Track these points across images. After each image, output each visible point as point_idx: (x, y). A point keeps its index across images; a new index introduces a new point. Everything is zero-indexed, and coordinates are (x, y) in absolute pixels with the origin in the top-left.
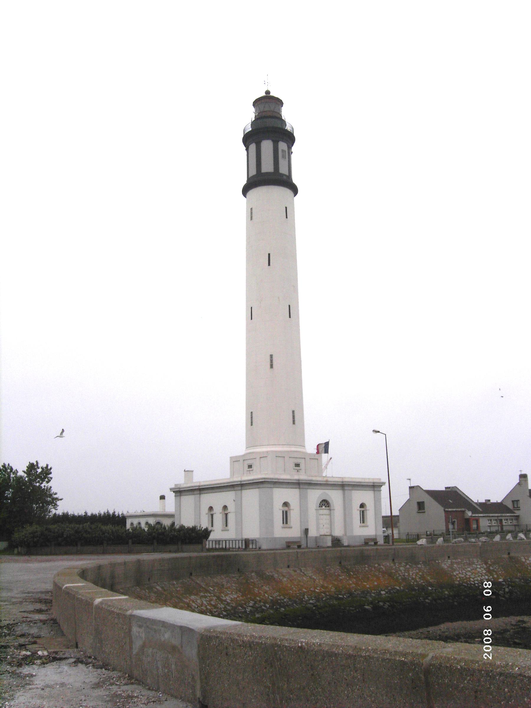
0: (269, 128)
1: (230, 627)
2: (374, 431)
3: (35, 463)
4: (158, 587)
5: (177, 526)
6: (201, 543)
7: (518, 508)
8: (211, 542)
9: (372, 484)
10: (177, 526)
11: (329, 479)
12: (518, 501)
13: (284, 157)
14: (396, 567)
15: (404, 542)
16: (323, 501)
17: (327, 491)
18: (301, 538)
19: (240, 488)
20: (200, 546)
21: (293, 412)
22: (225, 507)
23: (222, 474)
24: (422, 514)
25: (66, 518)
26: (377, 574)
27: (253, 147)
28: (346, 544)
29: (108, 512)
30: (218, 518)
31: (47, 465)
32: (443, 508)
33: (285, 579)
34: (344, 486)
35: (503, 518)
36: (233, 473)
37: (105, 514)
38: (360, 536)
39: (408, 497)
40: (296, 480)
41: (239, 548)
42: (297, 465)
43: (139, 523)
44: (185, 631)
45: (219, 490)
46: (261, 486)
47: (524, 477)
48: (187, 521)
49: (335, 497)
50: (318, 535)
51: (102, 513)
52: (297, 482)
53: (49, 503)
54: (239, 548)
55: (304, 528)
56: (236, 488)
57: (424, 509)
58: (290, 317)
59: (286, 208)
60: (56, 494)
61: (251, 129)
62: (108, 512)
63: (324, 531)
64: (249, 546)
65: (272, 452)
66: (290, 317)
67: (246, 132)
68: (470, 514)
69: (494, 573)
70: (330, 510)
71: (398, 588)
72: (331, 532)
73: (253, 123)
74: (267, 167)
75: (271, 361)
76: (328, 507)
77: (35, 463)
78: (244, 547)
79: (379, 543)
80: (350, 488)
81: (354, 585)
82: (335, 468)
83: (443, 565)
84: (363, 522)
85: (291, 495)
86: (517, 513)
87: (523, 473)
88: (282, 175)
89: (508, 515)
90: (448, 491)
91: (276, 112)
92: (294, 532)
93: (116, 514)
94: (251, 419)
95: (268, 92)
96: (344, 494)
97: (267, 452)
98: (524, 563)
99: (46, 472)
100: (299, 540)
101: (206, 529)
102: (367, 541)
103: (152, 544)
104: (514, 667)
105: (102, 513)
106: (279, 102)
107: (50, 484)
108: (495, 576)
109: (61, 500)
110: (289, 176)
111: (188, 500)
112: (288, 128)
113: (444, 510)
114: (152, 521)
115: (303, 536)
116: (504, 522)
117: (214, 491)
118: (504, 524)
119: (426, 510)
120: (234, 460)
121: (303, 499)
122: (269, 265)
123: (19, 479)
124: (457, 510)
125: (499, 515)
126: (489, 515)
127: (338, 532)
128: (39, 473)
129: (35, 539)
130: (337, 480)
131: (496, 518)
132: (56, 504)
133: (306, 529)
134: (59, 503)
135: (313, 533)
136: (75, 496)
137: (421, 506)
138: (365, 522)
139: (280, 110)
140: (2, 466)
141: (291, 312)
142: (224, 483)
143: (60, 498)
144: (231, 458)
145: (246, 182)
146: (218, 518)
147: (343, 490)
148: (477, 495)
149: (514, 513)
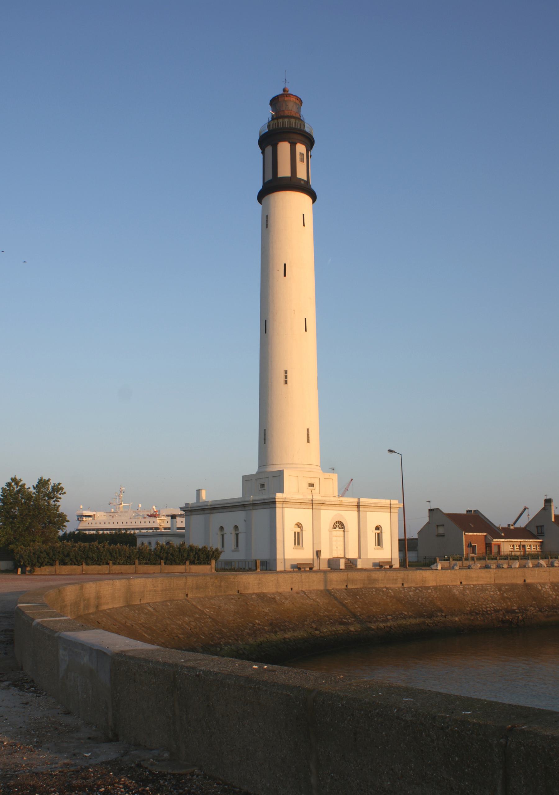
1: (152, 651)
4: (149, 608)
5: (187, 546)
10: (187, 546)
13: (302, 160)
14: (405, 592)
16: (339, 522)
17: (342, 513)
21: (308, 430)
22: (236, 527)
26: (385, 598)
27: (269, 149)
28: (359, 567)
30: (230, 539)
33: (287, 602)
39: (427, 520)
42: (312, 485)
43: (150, 543)
44: (99, 654)
47: (548, 501)
48: (196, 541)
56: (247, 508)
59: (304, 215)
61: (267, 130)
63: (338, 553)
69: (508, 600)
71: (406, 613)
76: (342, 528)
79: (394, 567)
81: (359, 609)
83: (455, 591)
84: (379, 545)
87: (548, 498)
89: (531, 540)
98: (540, 591)
101: (217, 550)
102: (379, 566)
103: (185, 564)
104: (393, 708)
108: (509, 603)
110: (308, 182)
111: (198, 519)
112: (307, 129)
114: (162, 541)
115: (315, 557)
116: (527, 548)
117: (225, 510)
120: (246, 479)
121: (315, 519)
125: (522, 540)
127: (352, 554)
135: (325, 555)
144: (243, 477)
145: (261, 188)
146: (230, 539)
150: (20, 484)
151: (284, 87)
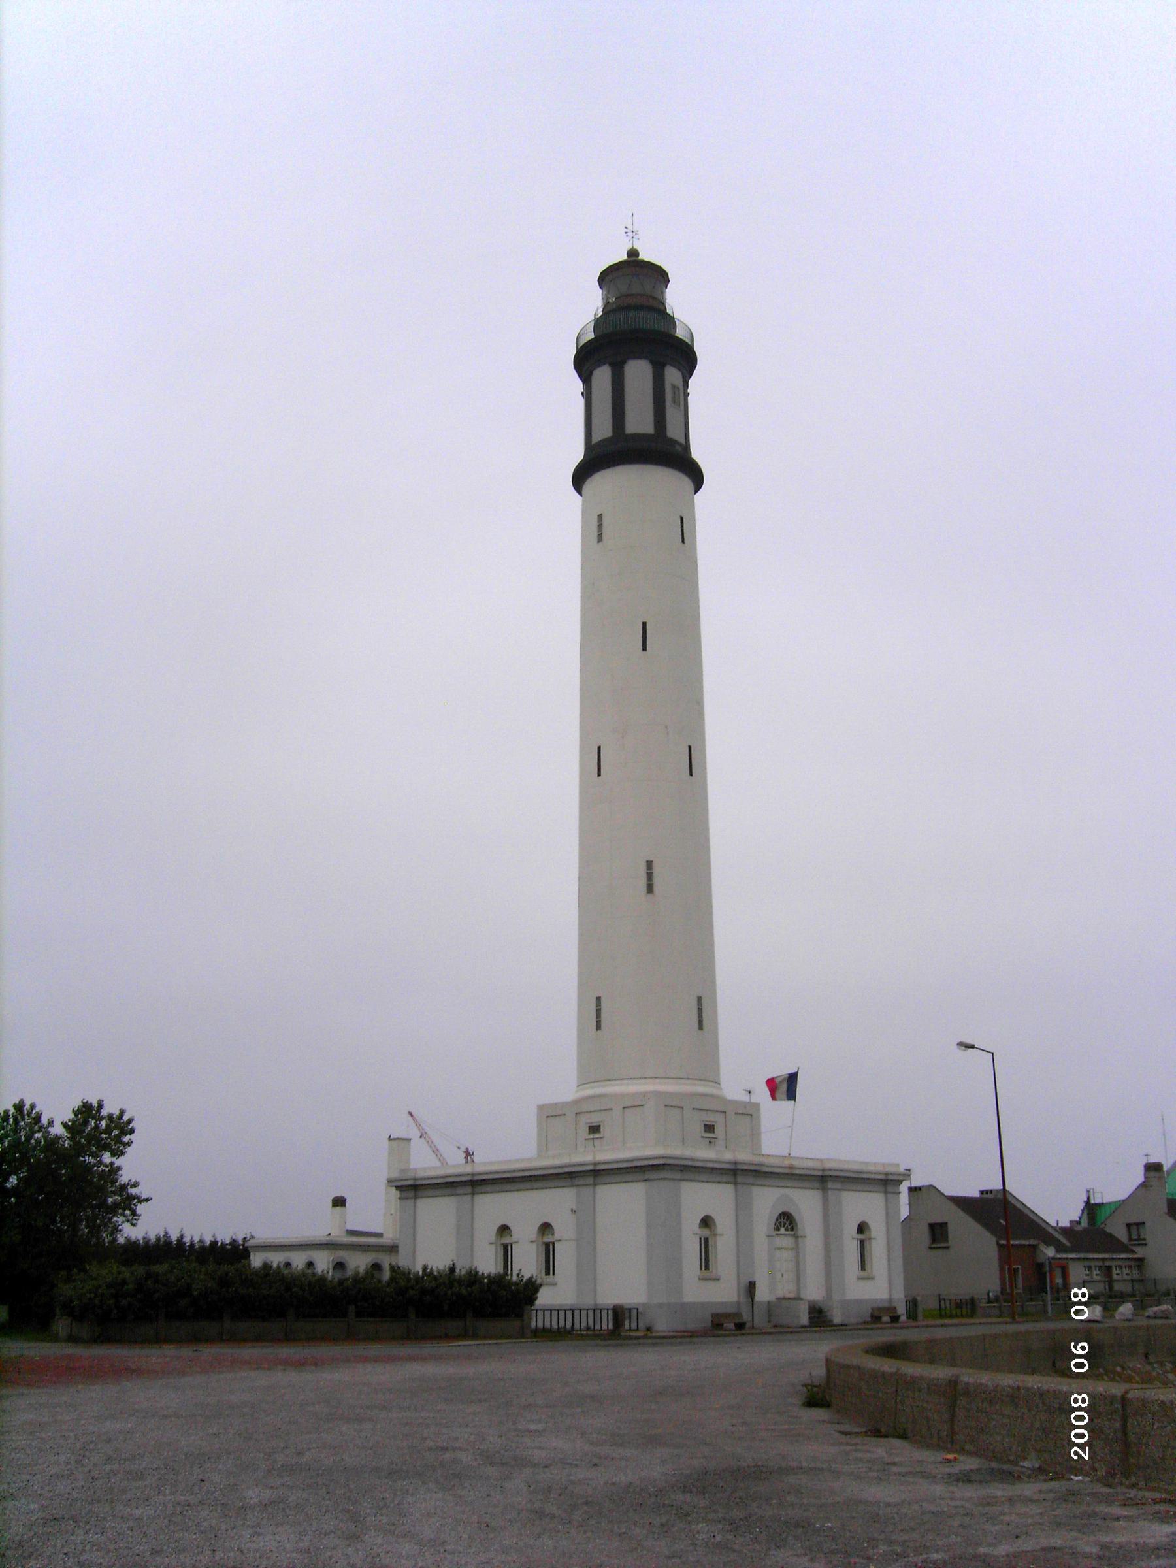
0: (635, 339)
2: (960, 1044)
3: (95, 1104)
6: (520, 1315)
7: (1142, 1242)
8: (540, 1313)
9: (882, 1177)
11: (796, 1163)
12: (1140, 1225)
15: (933, 1317)
17: (789, 1192)
18: (738, 1303)
19: (590, 1180)
20: (515, 1324)
22: (546, 1228)
23: (513, 1144)
24: (940, 1252)
25: (167, 1251)
29: (166, 1235)
30: (564, 1257)
31: (122, 1112)
32: (994, 1239)
34: (826, 1180)
35: (1113, 1264)
36: (544, 1142)
37: (158, 1239)
38: (859, 1302)
40: (729, 1163)
41: (588, 1328)
42: (709, 1128)
43: (310, 1264)
45: (528, 1185)
46: (653, 1175)
49: (806, 1204)
50: (772, 1298)
51: (153, 1238)
52: (732, 1167)
53: (114, 1209)
54: (588, 1328)
55: (745, 1281)
56: (577, 1182)
57: (947, 1241)
58: (691, 774)
60: (136, 1185)
62: (166, 1235)
63: (785, 1289)
64: (623, 1325)
65: (658, 1094)
66: (691, 774)
67: (581, 344)
68: (1050, 1252)
70: (796, 1237)
72: (798, 1290)
73: (598, 323)
74: (639, 421)
75: (650, 876)
76: (792, 1229)
77: (95, 1104)
78: (611, 1326)
80: (839, 1186)
82: (782, 1135)
85: (713, 1199)
86: (1140, 1252)
87: (1153, 1160)
88: (674, 442)
90: (987, 1200)
91: (654, 298)
92: (723, 1292)
93: (187, 1240)
94: (597, 1014)
95: (633, 253)
96: (886, 1200)
97: (644, 1094)
99: (119, 1131)
100: (733, 1310)
105: (153, 1238)
106: (659, 276)
107: (118, 1162)
109: (147, 1200)
110: (686, 447)
113: (998, 1244)
115: (744, 1299)
116: (1115, 1271)
118: (1115, 1277)
119: (951, 1242)
120: (549, 1114)
122: (644, 649)
123: (52, 1143)
124: (1023, 1242)
125: (1106, 1256)
126: (1091, 1256)
127: (814, 1292)
128: (100, 1130)
129: (124, 1302)
130: (810, 1164)
131: (1100, 1263)
132: (134, 1213)
133: (932, 1226)
134: (140, 1209)
135: (763, 1294)
136: (176, 1194)
137: (938, 1233)
138: (868, 1266)
139: (663, 293)
140: (15, 1106)
141: (693, 762)
142: (497, 1173)
143: (144, 1196)
147: (824, 1189)
148: (1058, 1208)
149: (1133, 1252)
150: (104, 1112)
151: (630, 247)
